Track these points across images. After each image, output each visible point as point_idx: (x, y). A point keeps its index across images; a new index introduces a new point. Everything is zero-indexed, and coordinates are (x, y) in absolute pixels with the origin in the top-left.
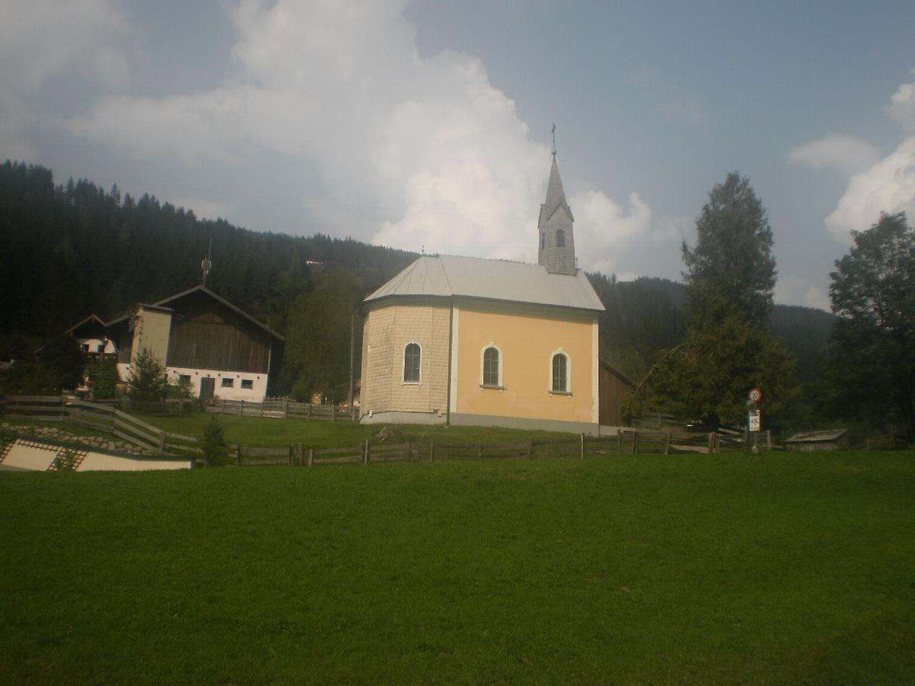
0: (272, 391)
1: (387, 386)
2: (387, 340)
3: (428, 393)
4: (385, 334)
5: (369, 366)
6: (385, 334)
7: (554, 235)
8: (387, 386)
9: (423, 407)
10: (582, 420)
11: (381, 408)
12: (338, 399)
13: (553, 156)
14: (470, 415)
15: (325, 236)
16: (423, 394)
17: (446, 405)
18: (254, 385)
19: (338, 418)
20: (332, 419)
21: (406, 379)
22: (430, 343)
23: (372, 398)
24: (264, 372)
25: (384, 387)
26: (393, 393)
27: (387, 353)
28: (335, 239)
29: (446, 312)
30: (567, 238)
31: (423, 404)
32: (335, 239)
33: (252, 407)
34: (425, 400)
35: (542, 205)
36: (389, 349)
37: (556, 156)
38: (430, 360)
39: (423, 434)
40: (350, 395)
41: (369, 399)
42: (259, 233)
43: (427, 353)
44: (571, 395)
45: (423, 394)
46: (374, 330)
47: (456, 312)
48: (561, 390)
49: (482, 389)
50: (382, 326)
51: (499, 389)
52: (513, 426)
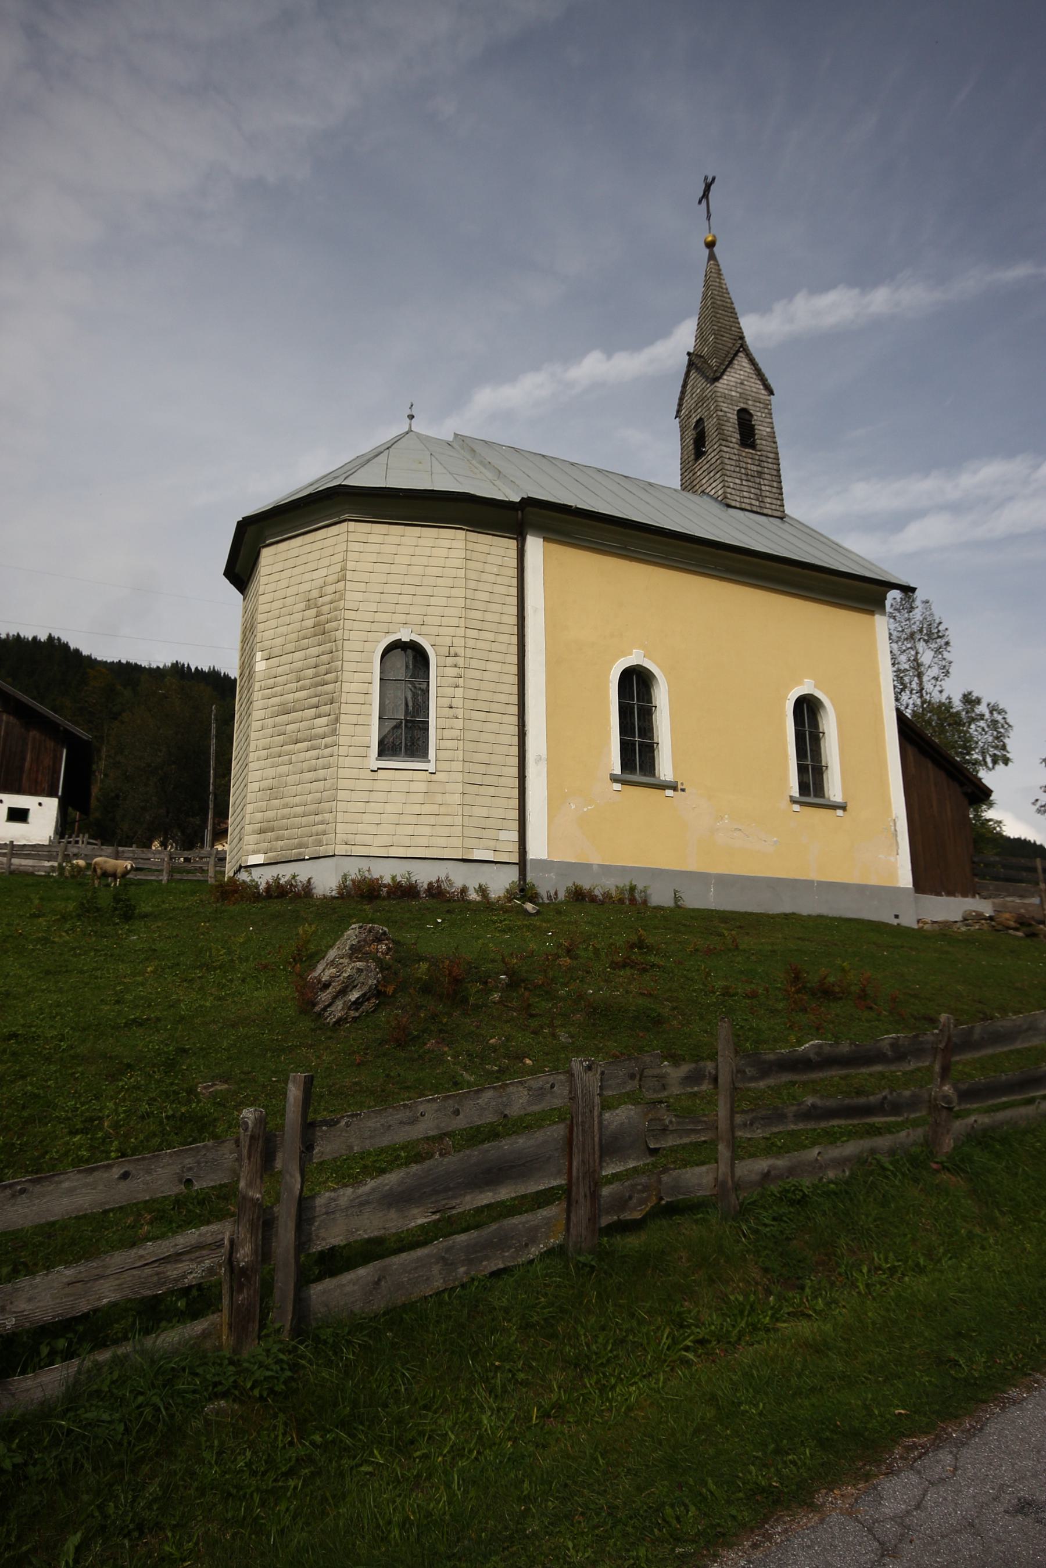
0: (64, 827)
1: (321, 773)
2: (321, 631)
3: (457, 798)
4: (313, 612)
5: (257, 714)
6: (313, 612)
7: (733, 417)
8: (321, 773)
9: (442, 842)
10: (873, 880)
11: (300, 846)
12: (191, 841)
13: (707, 251)
14: (589, 866)
15: (183, 665)
16: (439, 799)
17: (515, 836)
18: (31, 816)
19: (177, 876)
20: (164, 878)
21: (382, 753)
22: (459, 642)
23: (270, 814)
24: (51, 794)
25: (311, 775)
26: (342, 795)
27: (322, 669)
28: (197, 668)
29: (506, 547)
30: (761, 430)
31: (445, 831)
32: (197, 668)
33: (27, 856)
34: (448, 820)
35: (689, 354)
36: (325, 658)
37: (715, 249)
38: (459, 692)
39: (60, 829)
40: (208, 836)
41: (259, 816)
42: (106, 662)
43: (452, 672)
44: (843, 807)
45: (439, 799)
46: (277, 604)
47: (534, 545)
48: (816, 796)
49: (617, 786)
50: (305, 587)
51: (663, 786)
52: (808, 907)
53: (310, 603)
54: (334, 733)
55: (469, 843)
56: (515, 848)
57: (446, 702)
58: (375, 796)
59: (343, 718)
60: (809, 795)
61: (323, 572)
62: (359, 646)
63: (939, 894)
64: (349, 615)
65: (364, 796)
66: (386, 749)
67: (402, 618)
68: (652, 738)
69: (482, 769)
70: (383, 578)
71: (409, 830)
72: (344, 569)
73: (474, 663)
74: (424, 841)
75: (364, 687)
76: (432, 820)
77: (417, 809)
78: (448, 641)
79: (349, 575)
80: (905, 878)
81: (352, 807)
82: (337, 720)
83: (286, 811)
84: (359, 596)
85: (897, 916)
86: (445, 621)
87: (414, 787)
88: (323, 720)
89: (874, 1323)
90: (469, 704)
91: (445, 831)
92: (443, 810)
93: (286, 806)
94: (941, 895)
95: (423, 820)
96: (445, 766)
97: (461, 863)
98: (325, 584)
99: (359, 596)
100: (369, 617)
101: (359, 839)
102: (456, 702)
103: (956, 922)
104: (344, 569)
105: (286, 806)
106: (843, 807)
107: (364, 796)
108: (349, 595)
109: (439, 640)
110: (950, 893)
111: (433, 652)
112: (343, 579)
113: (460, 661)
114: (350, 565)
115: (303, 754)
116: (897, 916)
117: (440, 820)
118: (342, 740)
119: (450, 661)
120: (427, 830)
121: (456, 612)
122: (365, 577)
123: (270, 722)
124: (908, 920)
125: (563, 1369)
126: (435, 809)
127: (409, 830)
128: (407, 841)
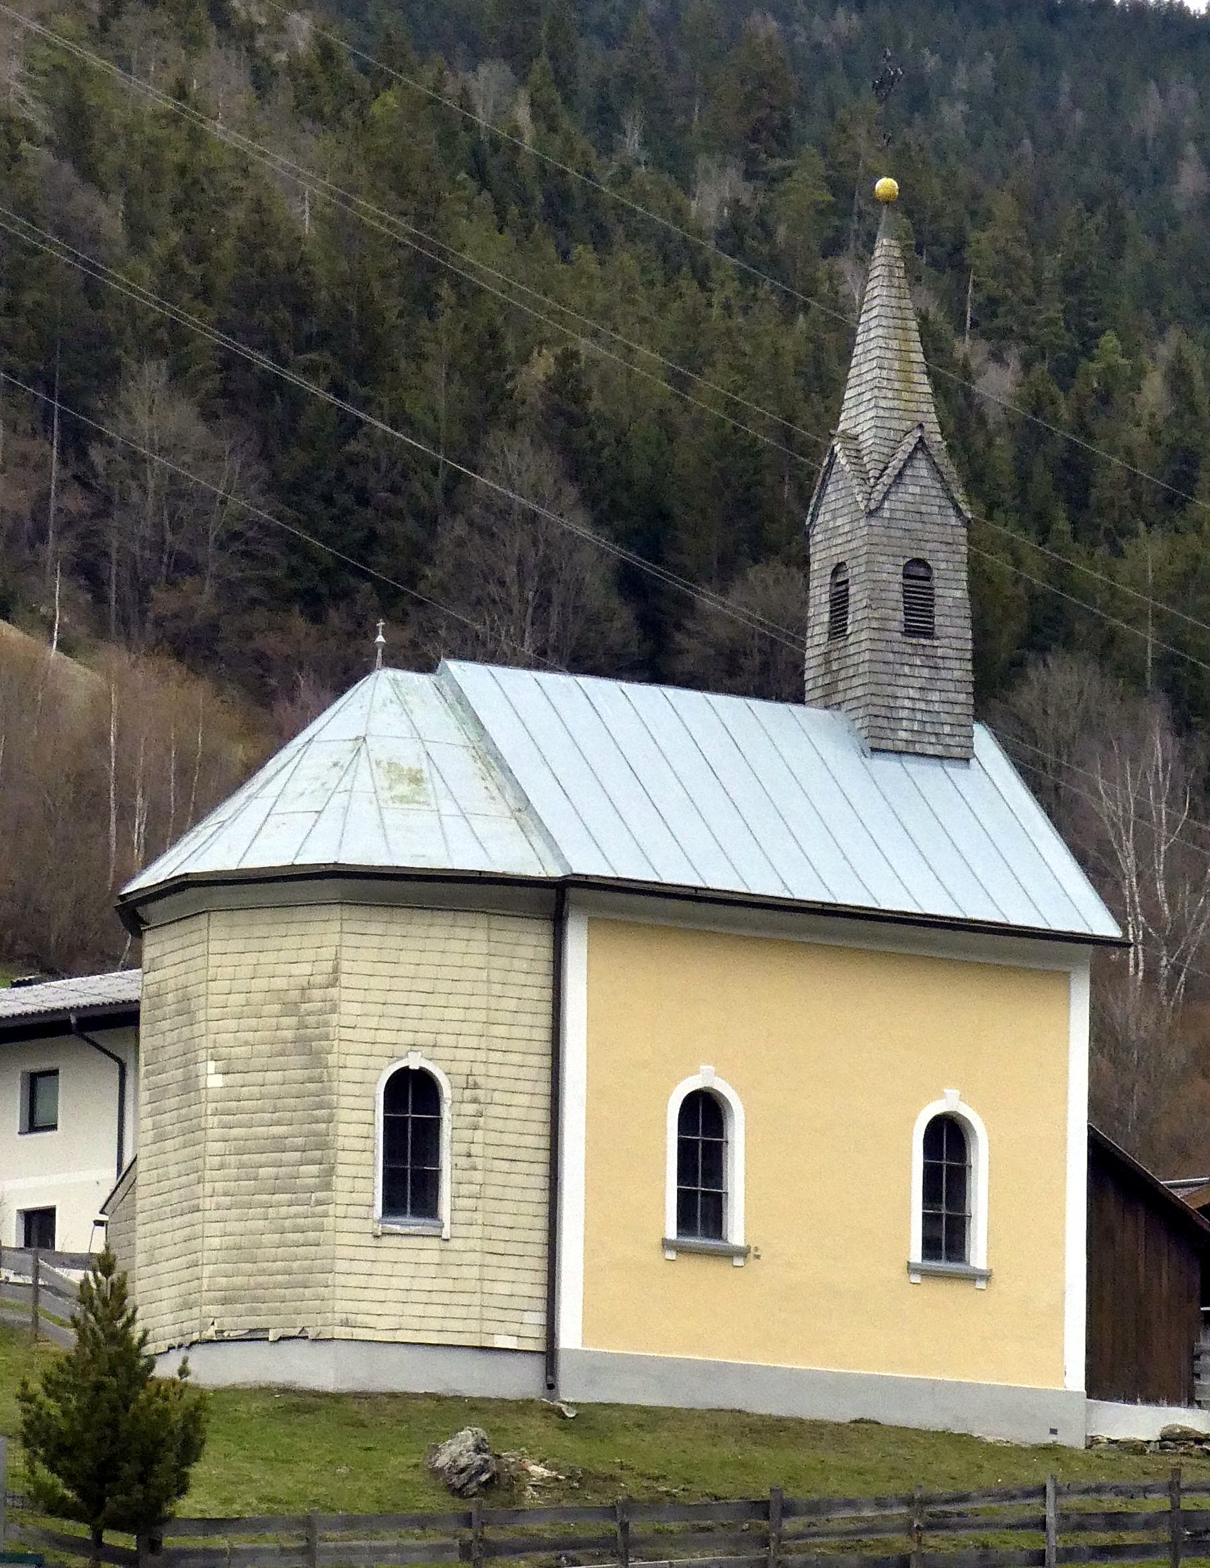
17: (539, 1318)
22: (479, 1069)
23: (238, 1281)
31: (462, 1312)
34: (464, 1299)
43: (471, 1108)
45: (454, 1272)
50: (280, 983)
53: (290, 1008)
54: (328, 1187)
55: (490, 1326)
56: (539, 1332)
57: (463, 1148)
58: (379, 1268)
59: (340, 1169)
60: (937, 1257)
61: (306, 969)
62: (356, 1075)
63: (1133, 1401)
64: (347, 1034)
65: (365, 1267)
66: (393, 1205)
67: (408, 1037)
68: (719, 1184)
69: (505, 1234)
70: (386, 983)
71: (419, 1310)
72: (336, 970)
73: (497, 1097)
74: (436, 1324)
75: (363, 1130)
76: (446, 1298)
77: (427, 1284)
78: (464, 1068)
79: (344, 980)
80: (1076, 1379)
81: (352, 1281)
82: (331, 1172)
83: (261, 1279)
84: (356, 1008)
85: (1054, 1432)
86: (462, 1041)
87: (424, 1257)
88: (314, 1169)
89: (301, 668)
90: (491, 1152)
91: (462, 1312)
92: (460, 1286)
93: (263, 1272)
94: (1135, 1403)
95: (435, 1297)
96: (462, 1231)
97: (479, 1355)
98: (310, 986)
99: (356, 1008)
100: (368, 1036)
101: (361, 1319)
102: (475, 1149)
103: (1149, 1442)
104: (336, 970)
105: (263, 1272)
106: (986, 1277)
107: (365, 1267)
108: (345, 1007)
109: (455, 1067)
110: (1150, 1399)
111: (447, 1081)
112: (333, 983)
113: (480, 1093)
114: (345, 966)
115: (284, 1208)
116: (1054, 1432)
117: (457, 1298)
118: (342, 1198)
119: (468, 1094)
120: (439, 1311)
121: (476, 1028)
122: (364, 982)
123: (233, 1159)
124: (1072, 1438)
125: (967, 119)
126: (449, 1284)
127: (419, 1310)
128: (416, 1323)
